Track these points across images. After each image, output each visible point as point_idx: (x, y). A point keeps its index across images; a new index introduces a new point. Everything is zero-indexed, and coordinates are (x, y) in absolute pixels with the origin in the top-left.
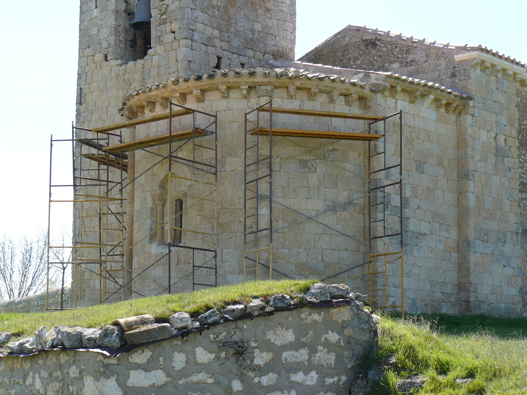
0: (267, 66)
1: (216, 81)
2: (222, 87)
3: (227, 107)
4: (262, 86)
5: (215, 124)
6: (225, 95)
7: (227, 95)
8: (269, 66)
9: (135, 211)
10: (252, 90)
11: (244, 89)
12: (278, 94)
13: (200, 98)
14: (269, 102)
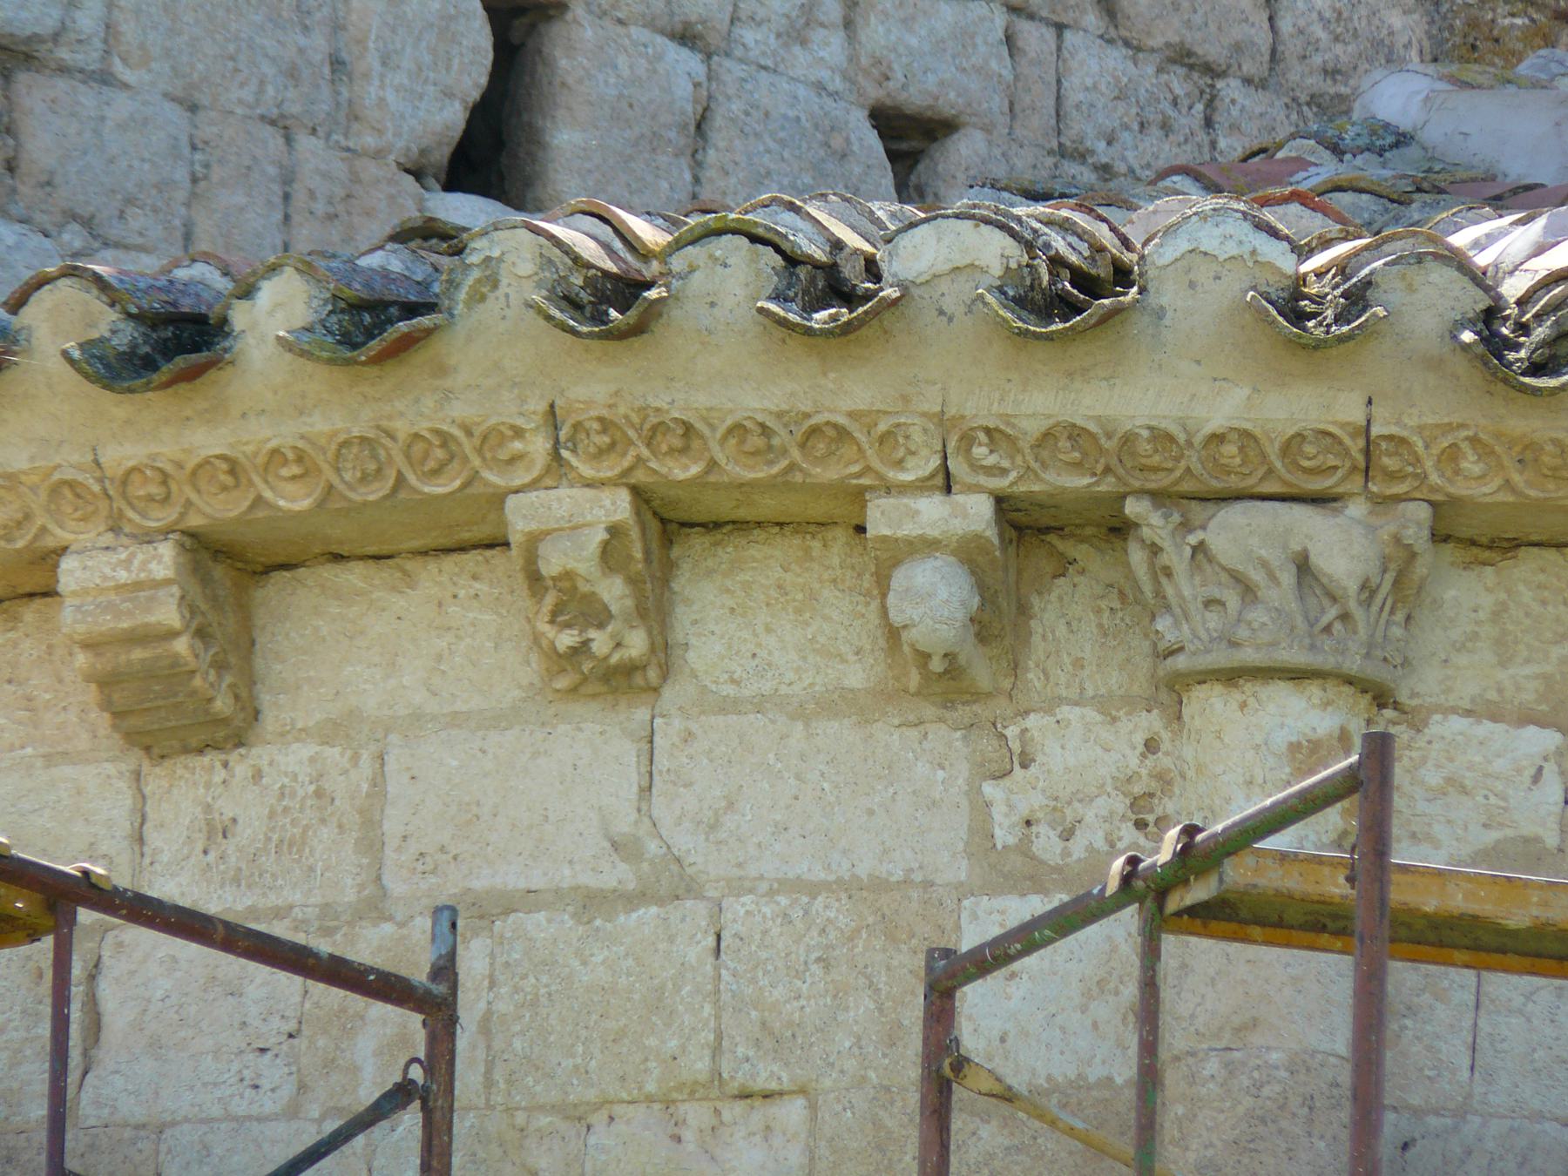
0: (1327, 169)
1: (460, 410)
2: (562, 502)
3: (622, 847)
4: (1234, 514)
5: (410, 1120)
6: (600, 642)
7: (637, 643)
8: (1369, 169)
9: (445, 711)
10: (1064, 566)
11: (926, 546)
12: (1504, 652)
13: (176, 673)
14: (1348, 785)
